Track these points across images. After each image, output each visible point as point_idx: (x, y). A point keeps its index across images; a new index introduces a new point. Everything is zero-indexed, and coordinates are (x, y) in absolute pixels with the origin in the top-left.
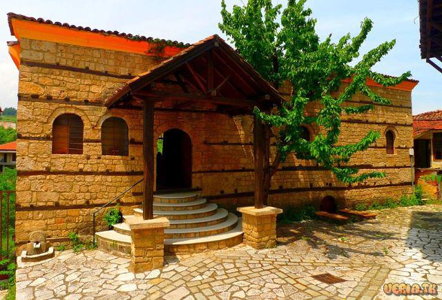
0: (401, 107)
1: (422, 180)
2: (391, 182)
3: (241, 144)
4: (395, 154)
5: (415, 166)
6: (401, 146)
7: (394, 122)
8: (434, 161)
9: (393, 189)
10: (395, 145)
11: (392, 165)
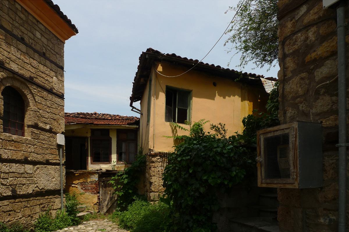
0: (43, 55)
1: (77, 188)
2: (14, 191)
3: (319, 123)
4: (28, 136)
5: (66, 164)
6: (41, 125)
7: (27, 75)
8: (91, 164)
9: (18, 204)
10: (29, 119)
11: (19, 156)
